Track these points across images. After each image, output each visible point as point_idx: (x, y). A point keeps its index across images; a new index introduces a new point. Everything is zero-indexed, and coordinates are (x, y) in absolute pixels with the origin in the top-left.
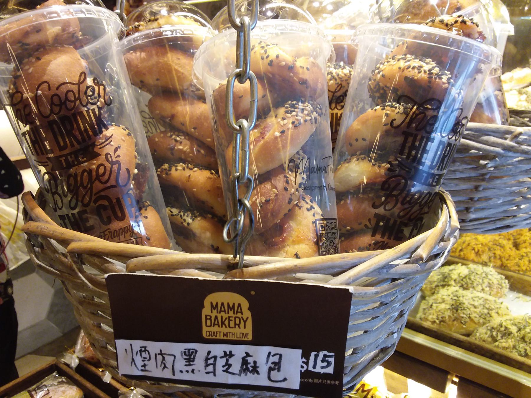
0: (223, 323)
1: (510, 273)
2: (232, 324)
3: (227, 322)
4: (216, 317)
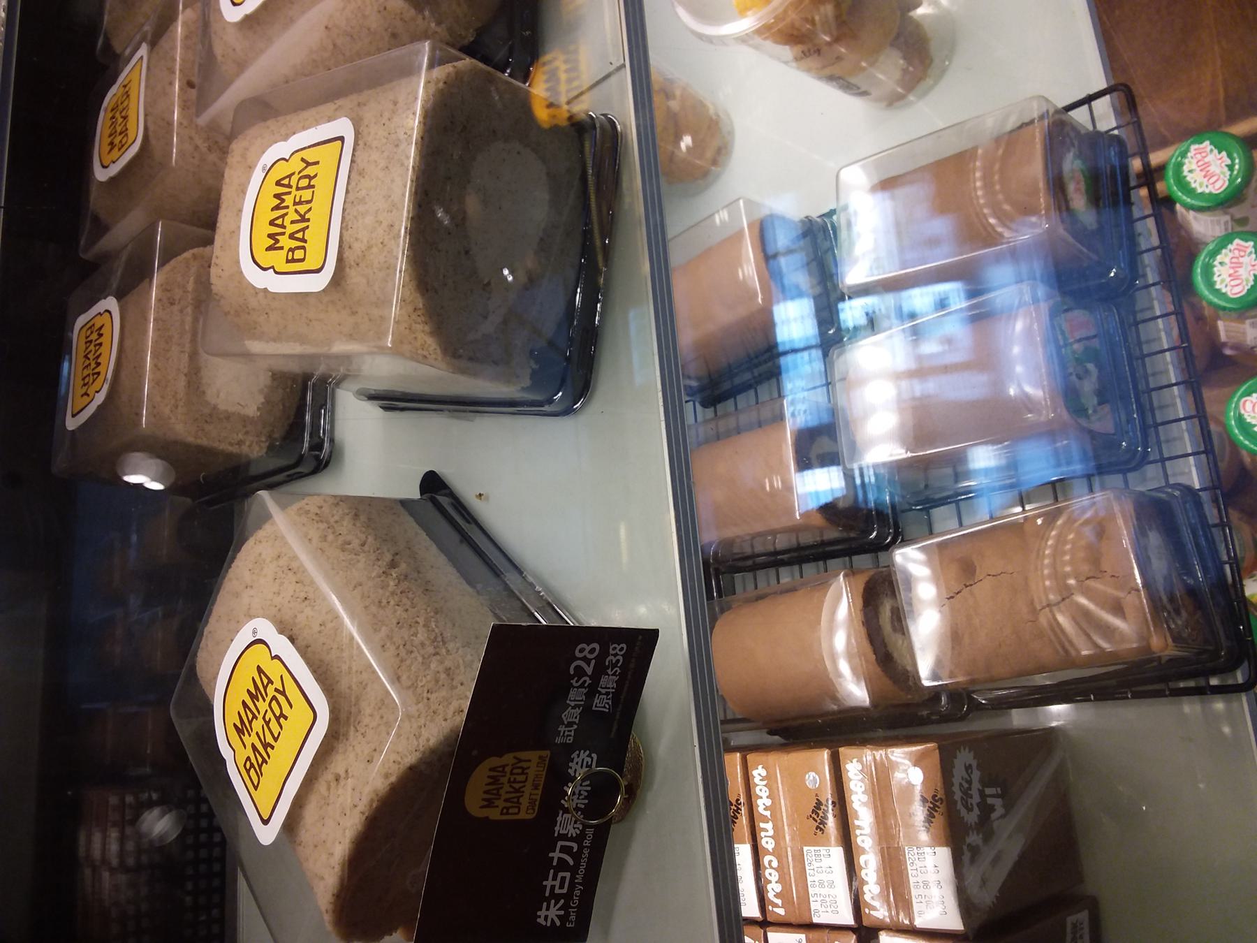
0: (517, 791)
2: (522, 778)
3: (517, 786)
4: (506, 800)
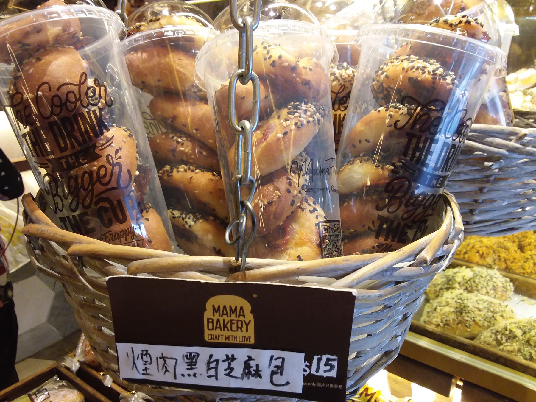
0: (225, 326)
1: (515, 276)
2: (234, 327)
3: (229, 326)
4: (218, 321)
